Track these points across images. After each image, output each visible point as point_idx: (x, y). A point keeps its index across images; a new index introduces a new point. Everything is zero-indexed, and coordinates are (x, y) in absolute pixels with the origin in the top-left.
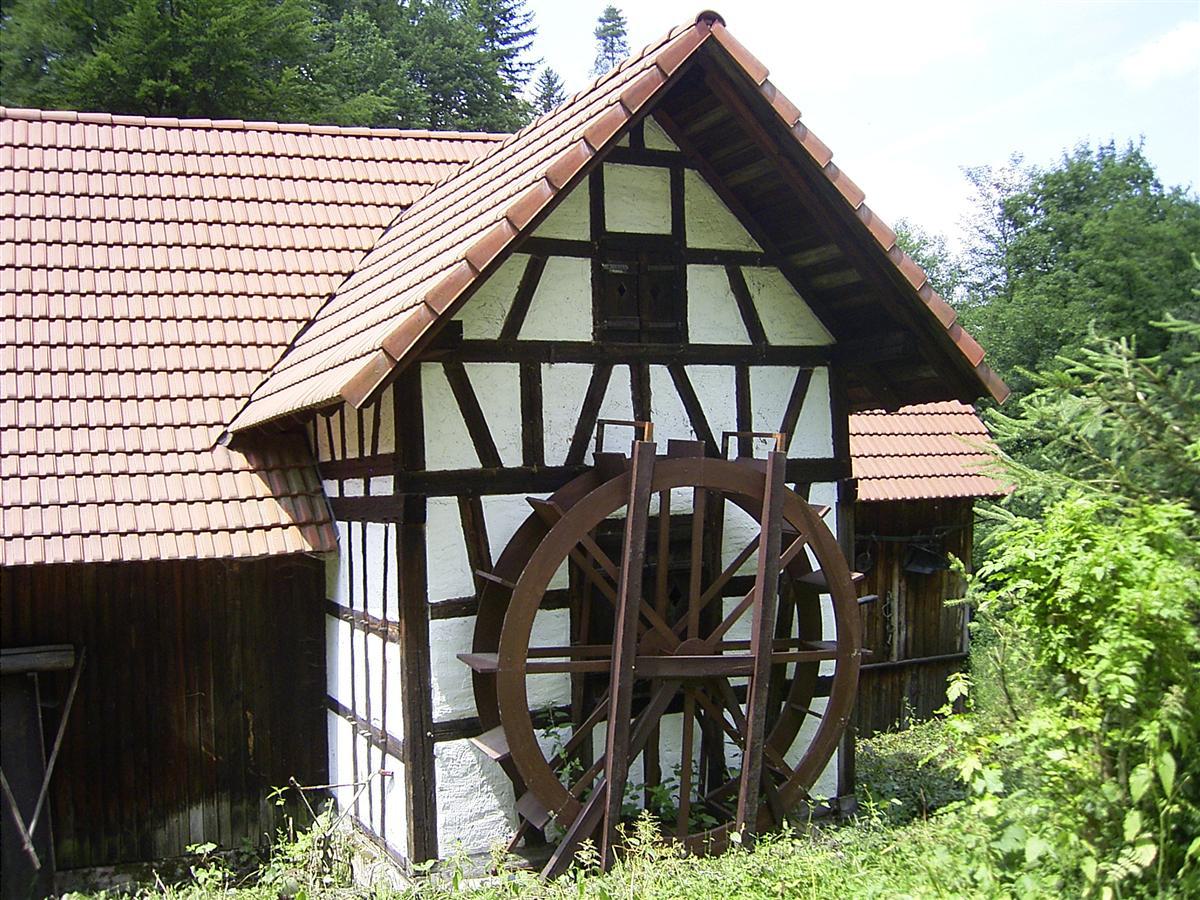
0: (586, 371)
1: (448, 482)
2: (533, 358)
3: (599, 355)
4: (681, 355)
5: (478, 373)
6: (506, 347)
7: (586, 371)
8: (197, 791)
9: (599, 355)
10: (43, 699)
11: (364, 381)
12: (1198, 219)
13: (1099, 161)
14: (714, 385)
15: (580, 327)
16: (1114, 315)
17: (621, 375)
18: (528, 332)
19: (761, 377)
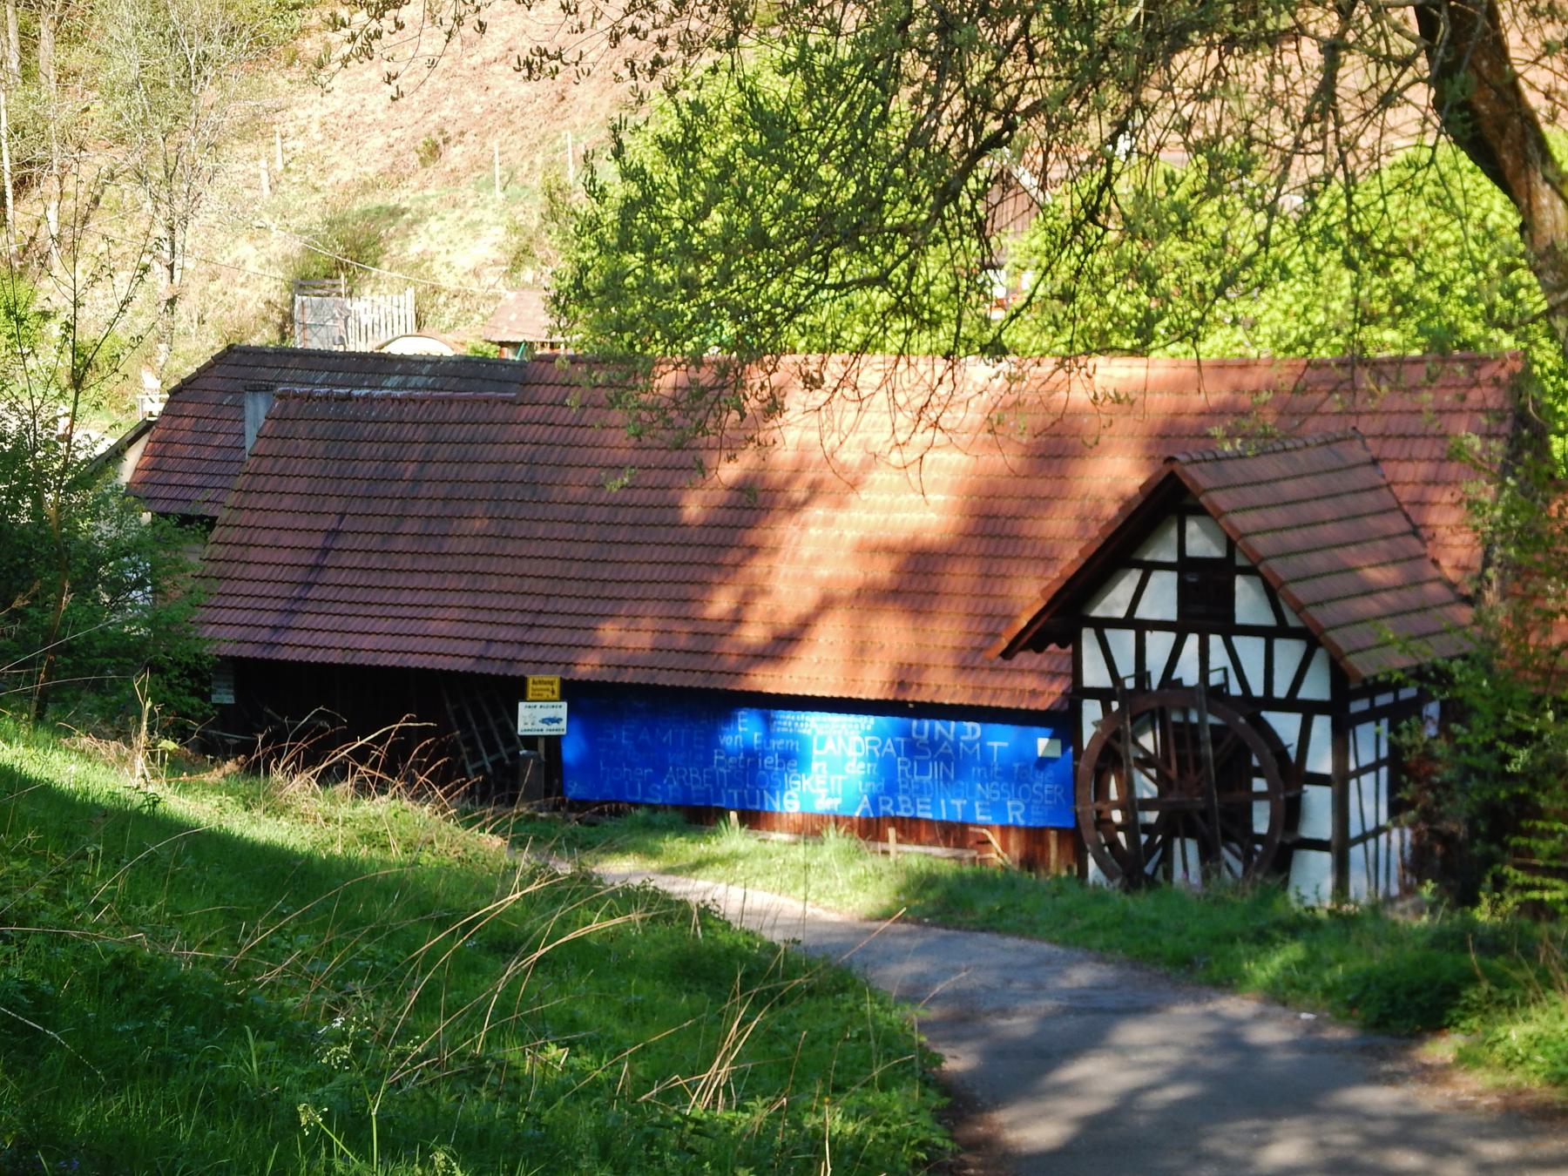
0: (1171, 637)
1: (1094, 693)
2: (1141, 628)
3: (1180, 629)
4: (1230, 630)
5: (1111, 635)
6: (1129, 622)
7: (1171, 637)
8: (1539, 557)
9: (1180, 629)
10: (257, 1039)
11: (111, 653)
12: (1566, 379)
13: (1267, 32)
14: (1251, 650)
15: (1171, 614)
16: (729, 472)
17: (1192, 641)
18: (1142, 613)
19: (1280, 645)
